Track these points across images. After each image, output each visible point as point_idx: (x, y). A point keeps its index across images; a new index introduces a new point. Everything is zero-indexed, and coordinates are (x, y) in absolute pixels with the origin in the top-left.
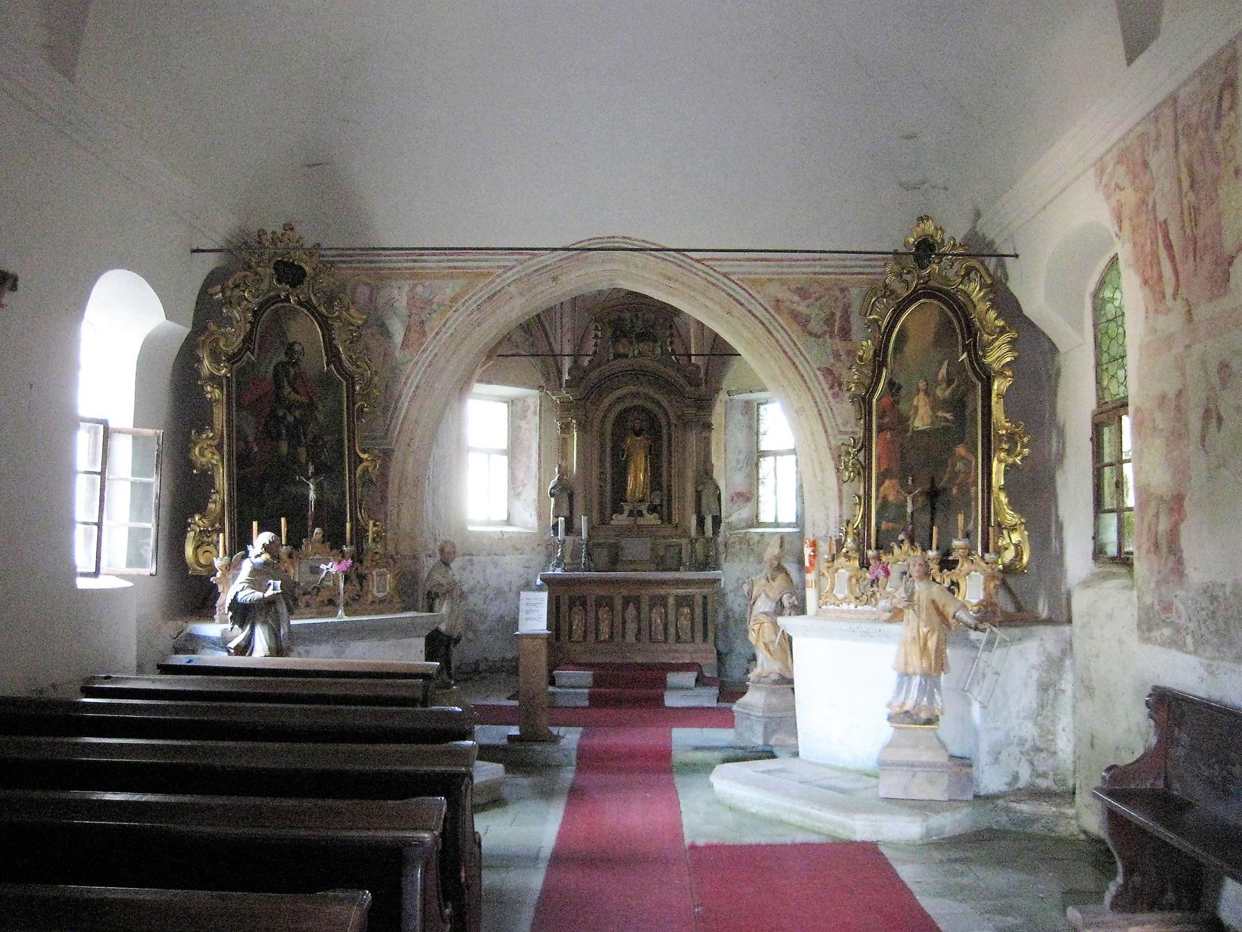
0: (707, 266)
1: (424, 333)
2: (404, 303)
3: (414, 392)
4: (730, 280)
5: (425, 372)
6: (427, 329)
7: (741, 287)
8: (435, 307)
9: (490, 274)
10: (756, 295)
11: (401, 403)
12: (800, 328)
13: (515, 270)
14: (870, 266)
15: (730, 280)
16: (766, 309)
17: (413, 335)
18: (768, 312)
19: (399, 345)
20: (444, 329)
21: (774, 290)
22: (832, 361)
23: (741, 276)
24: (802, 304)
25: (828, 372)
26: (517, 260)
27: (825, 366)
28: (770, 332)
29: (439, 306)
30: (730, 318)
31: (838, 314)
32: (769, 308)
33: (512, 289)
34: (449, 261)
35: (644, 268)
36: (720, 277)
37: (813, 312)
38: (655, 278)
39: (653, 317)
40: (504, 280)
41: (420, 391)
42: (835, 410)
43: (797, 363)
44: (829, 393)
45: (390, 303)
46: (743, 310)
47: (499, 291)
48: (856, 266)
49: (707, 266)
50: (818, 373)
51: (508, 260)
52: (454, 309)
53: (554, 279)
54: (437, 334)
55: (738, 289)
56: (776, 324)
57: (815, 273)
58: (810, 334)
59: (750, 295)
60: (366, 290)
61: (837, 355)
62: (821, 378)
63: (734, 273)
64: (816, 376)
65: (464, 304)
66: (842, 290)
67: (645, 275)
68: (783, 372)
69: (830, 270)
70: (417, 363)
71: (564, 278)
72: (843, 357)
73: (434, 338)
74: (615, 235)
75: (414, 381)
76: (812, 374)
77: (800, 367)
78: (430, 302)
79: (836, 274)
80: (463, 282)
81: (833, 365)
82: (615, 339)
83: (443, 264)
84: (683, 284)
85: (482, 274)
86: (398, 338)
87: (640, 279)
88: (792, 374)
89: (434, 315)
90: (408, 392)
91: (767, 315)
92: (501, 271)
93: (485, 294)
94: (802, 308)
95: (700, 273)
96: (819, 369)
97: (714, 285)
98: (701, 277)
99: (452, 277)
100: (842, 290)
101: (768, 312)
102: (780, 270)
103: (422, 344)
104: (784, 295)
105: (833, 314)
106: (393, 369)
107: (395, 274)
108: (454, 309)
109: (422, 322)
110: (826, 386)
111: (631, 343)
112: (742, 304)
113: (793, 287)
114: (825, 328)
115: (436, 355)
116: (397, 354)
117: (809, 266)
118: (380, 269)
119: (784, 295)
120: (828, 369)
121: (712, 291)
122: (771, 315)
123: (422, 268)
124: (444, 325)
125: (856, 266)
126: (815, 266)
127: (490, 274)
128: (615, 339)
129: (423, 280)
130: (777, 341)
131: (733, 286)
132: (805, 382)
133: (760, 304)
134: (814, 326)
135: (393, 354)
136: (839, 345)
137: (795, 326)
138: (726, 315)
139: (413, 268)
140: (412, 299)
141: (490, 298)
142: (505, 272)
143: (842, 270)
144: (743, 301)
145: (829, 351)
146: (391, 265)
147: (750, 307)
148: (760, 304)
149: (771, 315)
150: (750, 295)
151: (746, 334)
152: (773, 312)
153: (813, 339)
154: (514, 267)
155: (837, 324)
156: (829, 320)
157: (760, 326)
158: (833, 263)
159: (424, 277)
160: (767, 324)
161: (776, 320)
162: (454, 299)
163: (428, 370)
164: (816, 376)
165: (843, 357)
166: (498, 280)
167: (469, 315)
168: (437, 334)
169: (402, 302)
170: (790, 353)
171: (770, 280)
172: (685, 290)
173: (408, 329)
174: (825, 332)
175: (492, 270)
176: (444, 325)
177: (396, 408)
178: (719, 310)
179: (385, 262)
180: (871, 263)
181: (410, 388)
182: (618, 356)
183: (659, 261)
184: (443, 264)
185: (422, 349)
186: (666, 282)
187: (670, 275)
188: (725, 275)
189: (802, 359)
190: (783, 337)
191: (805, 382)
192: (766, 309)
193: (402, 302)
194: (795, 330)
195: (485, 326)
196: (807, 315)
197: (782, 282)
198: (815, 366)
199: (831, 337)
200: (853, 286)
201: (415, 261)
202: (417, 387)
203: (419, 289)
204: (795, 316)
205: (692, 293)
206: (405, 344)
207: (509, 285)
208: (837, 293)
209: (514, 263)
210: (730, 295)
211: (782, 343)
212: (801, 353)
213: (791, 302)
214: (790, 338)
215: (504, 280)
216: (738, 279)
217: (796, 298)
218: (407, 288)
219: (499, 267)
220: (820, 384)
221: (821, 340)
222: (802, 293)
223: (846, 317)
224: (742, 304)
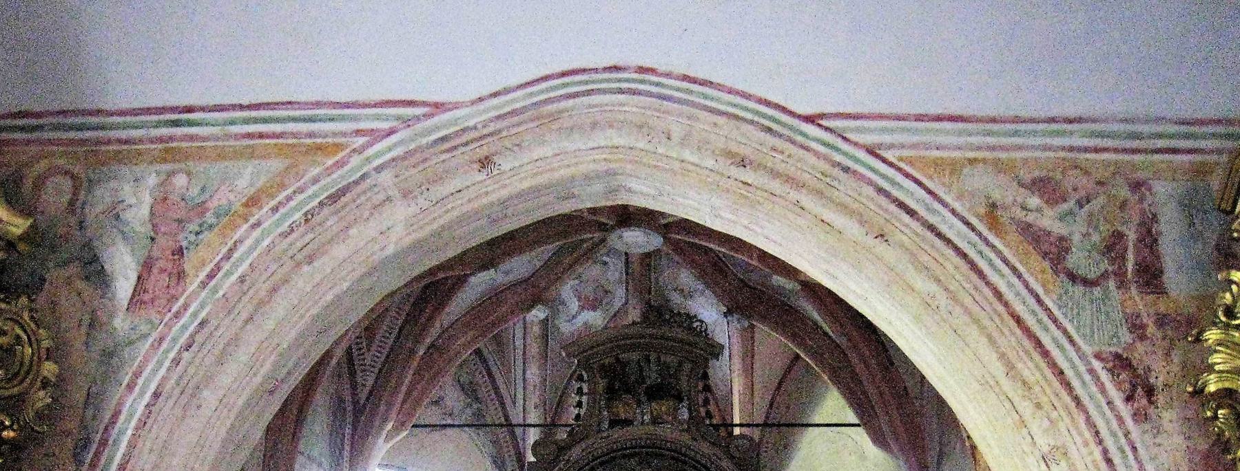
0: (827, 129)
1: (181, 276)
2: (145, 211)
3: (147, 406)
4: (884, 161)
5: (176, 361)
6: (187, 267)
7: (907, 175)
8: (210, 218)
9: (338, 147)
10: (941, 193)
11: (116, 430)
12: (1046, 264)
13: (394, 139)
14: (1187, 136)
15: (884, 161)
16: (967, 224)
17: (158, 281)
18: (973, 229)
19: (125, 303)
20: (226, 266)
21: (983, 182)
22: (1126, 337)
23: (906, 153)
24: (1049, 212)
25: (1120, 363)
26: (398, 118)
27: (1113, 349)
28: (980, 274)
29: (218, 216)
30: (880, 248)
31: (1132, 236)
32: (974, 221)
33: (386, 177)
34: (246, 121)
35: (684, 141)
36: (862, 155)
37: (1075, 231)
38: (710, 163)
39: (936, 318)
40: (368, 160)
41: (166, 407)
42: (1141, 451)
43: (1046, 341)
44: (1125, 411)
45: (115, 214)
46: (915, 225)
47: (356, 183)
48: (1160, 136)
49: (827, 129)
50: (1097, 365)
51: (378, 118)
52: (252, 220)
53: (485, 163)
54: (211, 276)
55: (899, 178)
56: (992, 256)
57: (1071, 149)
58: (1073, 277)
59: (930, 192)
60: (67, 184)
61: (1137, 328)
62: (1104, 376)
63: (891, 146)
64: (1091, 371)
65: (275, 209)
66: (1137, 186)
67: (687, 155)
68: (1013, 367)
69: (1109, 143)
70: (161, 340)
71: (506, 163)
72: (1151, 329)
73: (204, 285)
74: (621, 63)
75: (149, 384)
76: (1082, 369)
77: (1055, 353)
78: (201, 208)
79: (1116, 150)
80: (276, 165)
81: (1130, 347)
82: (612, 394)
83: (235, 129)
84: (775, 174)
85: (319, 148)
86: (124, 287)
87: (677, 165)
88: (1033, 369)
89: (206, 236)
90: (135, 406)
91: (972, 235)
92: (361, 141)
93: (316, 193)
94: (1048, 220)
95: (814, 145)
96: (1098, 356)
97: (846, 170)
98: (817, 154)
99: (251, 154)
100: (1137, 186)
101: (973, 229)
102: (991, 140)
103: (175, 298)
104: (1004, 191)
105: (1119, 236)
106: (108, 355)
107: (127, 153)
108: (252, 220)
109: (180, 252)
110: (1117, 398)
111: (639, 403)
112: (911, 213)
113: (1027, 177)
114: (1105, 265)
115: (203, 324)
116: (120, 323)
117: (1058, 134)
118: (98, 142)
119: (1004, 191)
120: (1117, 356)
121: (846, 188)
122: (980, 235)
123: (192, 138)
124: (228, 257)
125: (1160, 136)
126: (1071, 133)
127: (338, 147)
128: (612, 394)
129: (191, 163)
130: (998, 295)
131: (891, 172)
132: (1068, 386)
133: (953, 212)
134: (1077, 259)
135: (109, 323)
136: (1139, 301)
137: (1037, 262)
138: (870, 241)
139: (171, 139)
140: (162, 200)
141: (334, 198)
142: (370, 144)
143: (1129, 144)
144: (913, 205)
145: (1117, 316)
146: (123, 134)
147: (932, 219)
148: (953, 212)
149: (980, 235)
150: (930, 192)
151: (922, 284)
152: (980, 227)
153: (1079, 290)
154: (391, 132)
155: (1131, 256)
156: (1113, 246)
157: (958, 261)
158: (1032, 141)
159: (186, 156)
160: (972, 254)
161: (993, 247)
162: (253, 202)
163: (186, 355)
164: (1091, 371)
165: (1151, 329)
166: (356, 160)
167: (285, 235)
168: (211, 276)
169: (138, 212)
170: (1030, 321)
171: (972, 161)
172: (776, 186)
173: (147, 266)
174: (1105, 276)
175: (343, 140)
176: (228, 257)
177: (104, 443)
178: (852, 229)
179: (126, 127)
180: (1192, 129)
181: (142, 393)
182: (614, 423)
183: (721, 120)
184: (235, 129)
185: (174, 309)
186: (735, 172)
187: (743, 151)
188: (871, 151)
189: (1058, 334)
190: (1010, 285)
191: (1068, 386)
192: (967, 224)
193: (138, 212)
194: (1036, 270)
195: (324, 264)
196: (1062, 239)
197: (999, 167)
198: (1087, 349)
199: (1122, 285)
200: (1157, 175)
201: (176, 123)
202: (156, 395)
203: (180, 181)
204: (1033, 236)
205: (794, 195)
206: (137, 299)
207: (379, 169)
208: (1124, 193)
209: (395, 124)
210: (887, 195)
211: (1009, 296)
212: (1055, 321)
213: (1024, 208)
214: (1027, 286)
215: (368, 160)
216: (901, 159)
217: (1034, 201)
218: (152, 180)
219: (358, 132)
220: (1103, 391)
221: (1097, 291)
222: (1047, 188)
223: (1149, 239)
224: (911, 213)
